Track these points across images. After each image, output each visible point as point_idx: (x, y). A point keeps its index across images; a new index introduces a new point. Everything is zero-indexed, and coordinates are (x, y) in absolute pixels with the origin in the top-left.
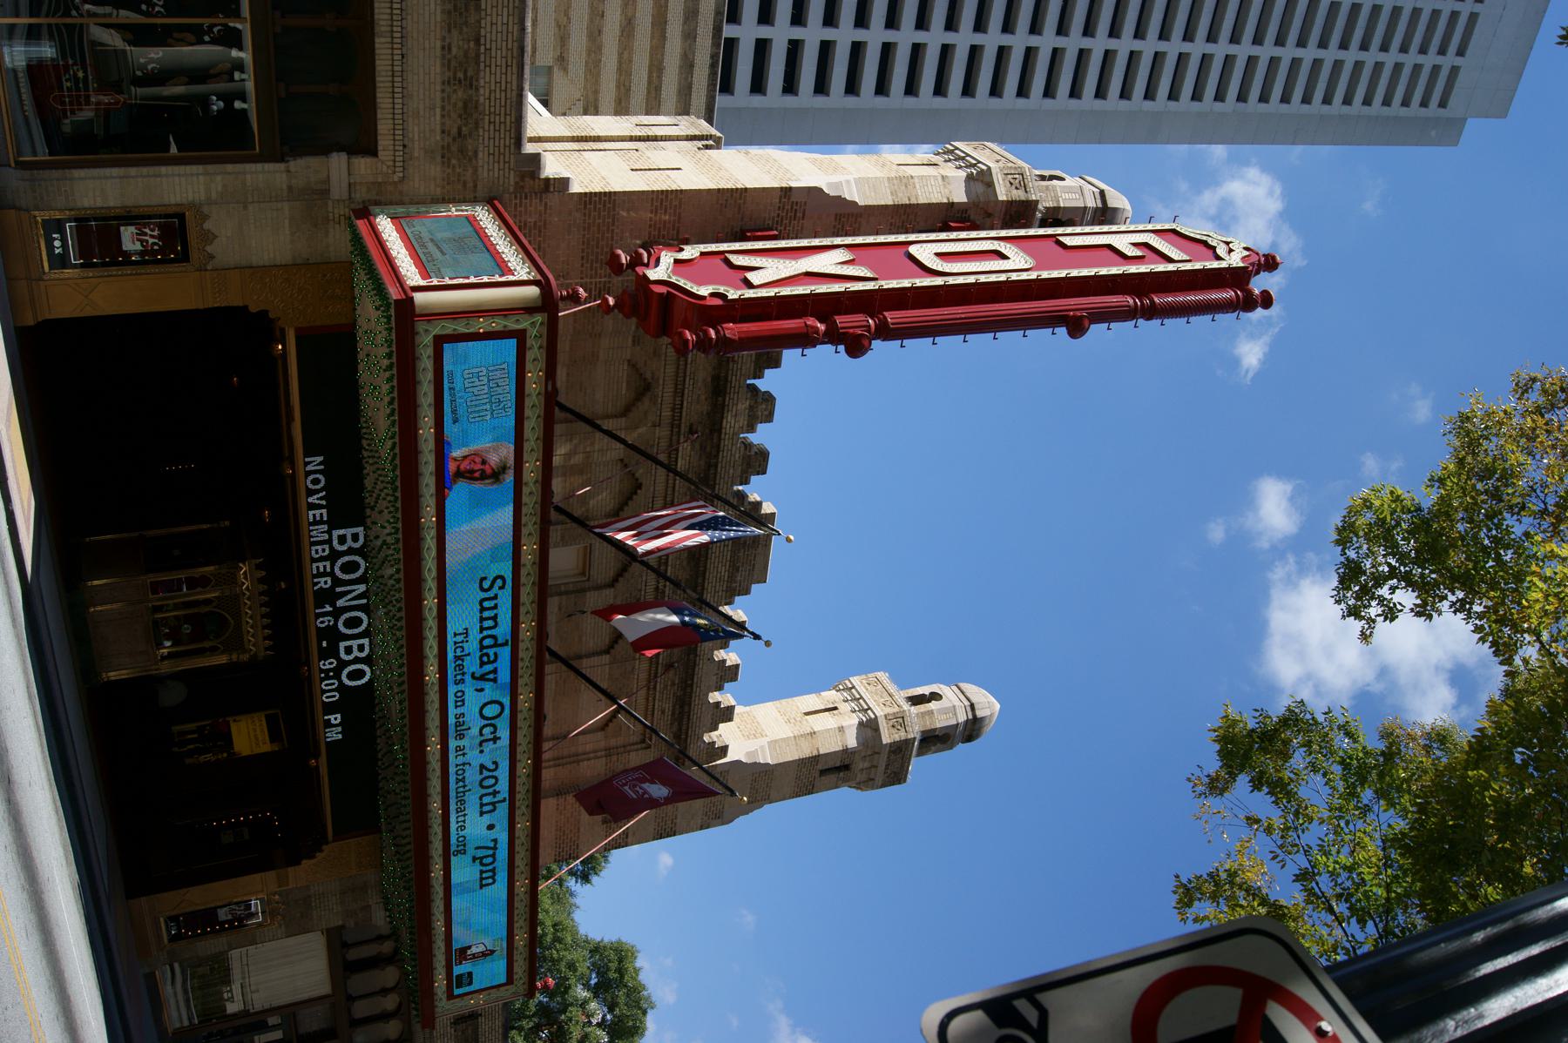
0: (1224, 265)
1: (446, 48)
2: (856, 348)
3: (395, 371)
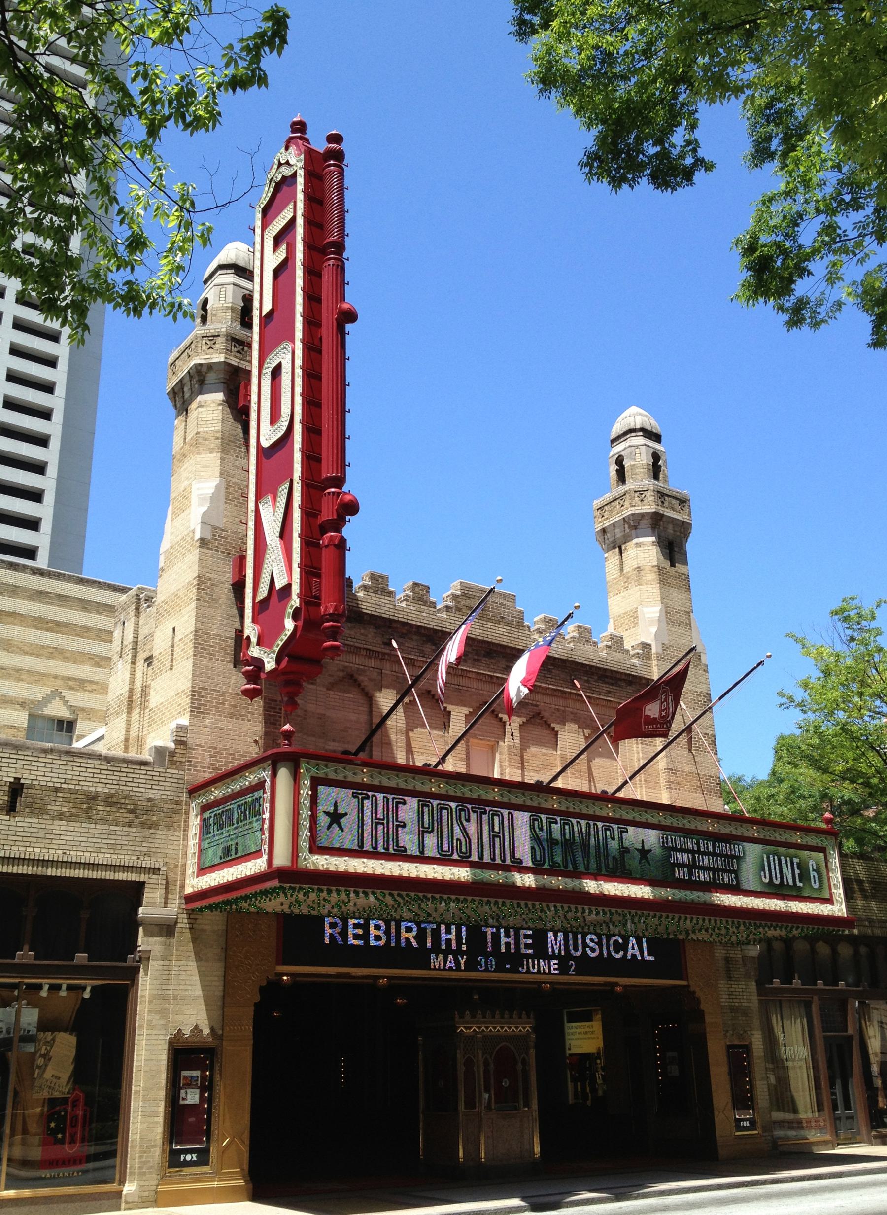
0: (301, 172)
1: (61, 816)
3: (361, 890)
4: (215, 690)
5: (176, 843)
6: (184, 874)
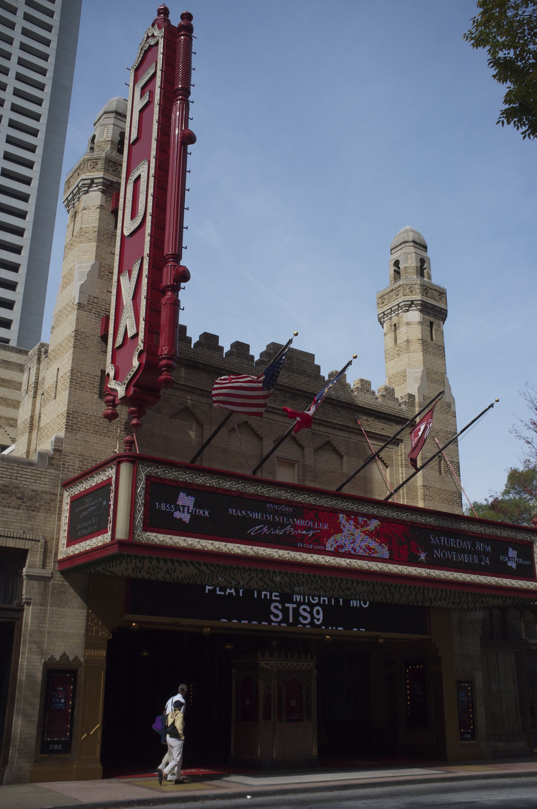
0: (161, 42)
2: (184, 276)
4: (85, 414)
5: (52, 523)
6: (57, 546)
